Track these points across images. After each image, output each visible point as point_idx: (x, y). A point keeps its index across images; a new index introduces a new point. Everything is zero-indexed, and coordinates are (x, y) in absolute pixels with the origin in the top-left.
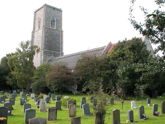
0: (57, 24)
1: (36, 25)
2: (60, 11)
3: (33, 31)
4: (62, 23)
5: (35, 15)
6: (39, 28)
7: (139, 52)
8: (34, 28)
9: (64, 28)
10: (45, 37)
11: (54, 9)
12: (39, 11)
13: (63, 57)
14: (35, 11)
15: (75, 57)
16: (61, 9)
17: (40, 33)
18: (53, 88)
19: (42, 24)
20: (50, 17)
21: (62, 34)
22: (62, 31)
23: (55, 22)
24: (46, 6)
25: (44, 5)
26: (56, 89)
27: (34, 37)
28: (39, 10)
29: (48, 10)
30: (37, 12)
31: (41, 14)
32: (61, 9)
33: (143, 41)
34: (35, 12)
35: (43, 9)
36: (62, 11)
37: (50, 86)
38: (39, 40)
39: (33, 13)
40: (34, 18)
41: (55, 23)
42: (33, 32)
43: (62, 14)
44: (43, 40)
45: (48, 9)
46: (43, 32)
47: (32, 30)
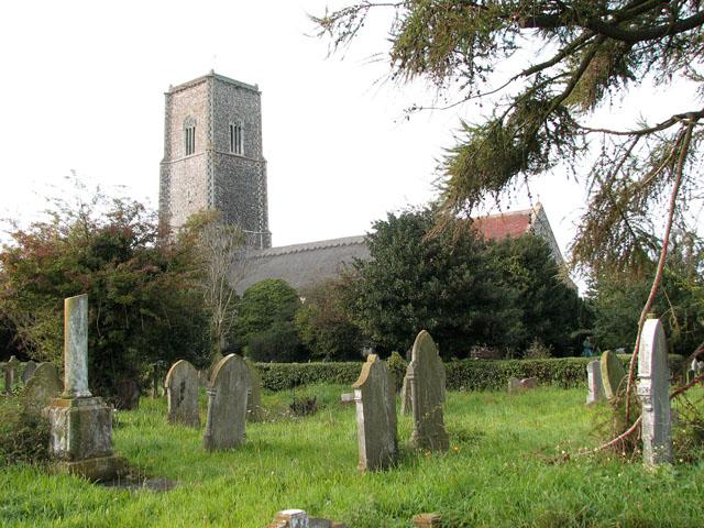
0: (246, 140)
1: (174, 139)
2: (253, 92)
3: (164, 160)
4: (260, 133)
5: (169, 103)
6: (190, 149)
7: (539, 268)
8: (168, 149)
9: (270, 149)
10: (216, 184)
11: (238, 87)
12: (184, 93)
13: (268, 252)
14: (167, 92)
15: (330, 252)
16: (256, 87)
17: (197, 170)
18: (325, 345)
19: (202, 140)
20: (228, 115)
21: (264, 171)
22: (263, 162)
23: (242, 131)
24: (214, 78)
25: (208, 77)
26: (333, 351)
27: (169, 180)
28: (185, 88)
29: (219, 92)
30: (175, 96)
31: (197, 108)
32: (256, 87)
33: (17, 245)
34: (169, 95)
35: (204, 87)
36: (259, 94)
37: (314, 341)
38: (191, 194)
39: (163, 100)
40: (167, 113)
41: (242, 137)
42: (166, 163)
43: (260, 104)
44: (212, 194)
45: (222, 90)
46: (211, 167)
47: (161, 155)
